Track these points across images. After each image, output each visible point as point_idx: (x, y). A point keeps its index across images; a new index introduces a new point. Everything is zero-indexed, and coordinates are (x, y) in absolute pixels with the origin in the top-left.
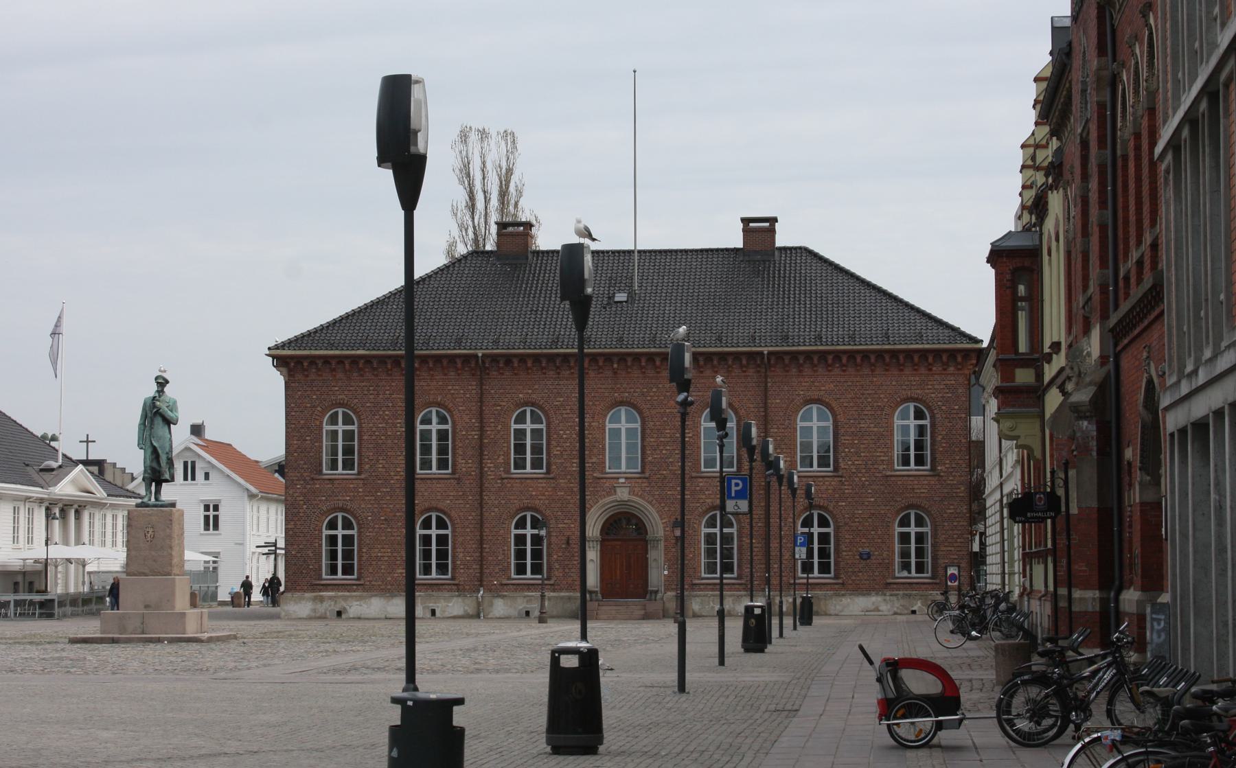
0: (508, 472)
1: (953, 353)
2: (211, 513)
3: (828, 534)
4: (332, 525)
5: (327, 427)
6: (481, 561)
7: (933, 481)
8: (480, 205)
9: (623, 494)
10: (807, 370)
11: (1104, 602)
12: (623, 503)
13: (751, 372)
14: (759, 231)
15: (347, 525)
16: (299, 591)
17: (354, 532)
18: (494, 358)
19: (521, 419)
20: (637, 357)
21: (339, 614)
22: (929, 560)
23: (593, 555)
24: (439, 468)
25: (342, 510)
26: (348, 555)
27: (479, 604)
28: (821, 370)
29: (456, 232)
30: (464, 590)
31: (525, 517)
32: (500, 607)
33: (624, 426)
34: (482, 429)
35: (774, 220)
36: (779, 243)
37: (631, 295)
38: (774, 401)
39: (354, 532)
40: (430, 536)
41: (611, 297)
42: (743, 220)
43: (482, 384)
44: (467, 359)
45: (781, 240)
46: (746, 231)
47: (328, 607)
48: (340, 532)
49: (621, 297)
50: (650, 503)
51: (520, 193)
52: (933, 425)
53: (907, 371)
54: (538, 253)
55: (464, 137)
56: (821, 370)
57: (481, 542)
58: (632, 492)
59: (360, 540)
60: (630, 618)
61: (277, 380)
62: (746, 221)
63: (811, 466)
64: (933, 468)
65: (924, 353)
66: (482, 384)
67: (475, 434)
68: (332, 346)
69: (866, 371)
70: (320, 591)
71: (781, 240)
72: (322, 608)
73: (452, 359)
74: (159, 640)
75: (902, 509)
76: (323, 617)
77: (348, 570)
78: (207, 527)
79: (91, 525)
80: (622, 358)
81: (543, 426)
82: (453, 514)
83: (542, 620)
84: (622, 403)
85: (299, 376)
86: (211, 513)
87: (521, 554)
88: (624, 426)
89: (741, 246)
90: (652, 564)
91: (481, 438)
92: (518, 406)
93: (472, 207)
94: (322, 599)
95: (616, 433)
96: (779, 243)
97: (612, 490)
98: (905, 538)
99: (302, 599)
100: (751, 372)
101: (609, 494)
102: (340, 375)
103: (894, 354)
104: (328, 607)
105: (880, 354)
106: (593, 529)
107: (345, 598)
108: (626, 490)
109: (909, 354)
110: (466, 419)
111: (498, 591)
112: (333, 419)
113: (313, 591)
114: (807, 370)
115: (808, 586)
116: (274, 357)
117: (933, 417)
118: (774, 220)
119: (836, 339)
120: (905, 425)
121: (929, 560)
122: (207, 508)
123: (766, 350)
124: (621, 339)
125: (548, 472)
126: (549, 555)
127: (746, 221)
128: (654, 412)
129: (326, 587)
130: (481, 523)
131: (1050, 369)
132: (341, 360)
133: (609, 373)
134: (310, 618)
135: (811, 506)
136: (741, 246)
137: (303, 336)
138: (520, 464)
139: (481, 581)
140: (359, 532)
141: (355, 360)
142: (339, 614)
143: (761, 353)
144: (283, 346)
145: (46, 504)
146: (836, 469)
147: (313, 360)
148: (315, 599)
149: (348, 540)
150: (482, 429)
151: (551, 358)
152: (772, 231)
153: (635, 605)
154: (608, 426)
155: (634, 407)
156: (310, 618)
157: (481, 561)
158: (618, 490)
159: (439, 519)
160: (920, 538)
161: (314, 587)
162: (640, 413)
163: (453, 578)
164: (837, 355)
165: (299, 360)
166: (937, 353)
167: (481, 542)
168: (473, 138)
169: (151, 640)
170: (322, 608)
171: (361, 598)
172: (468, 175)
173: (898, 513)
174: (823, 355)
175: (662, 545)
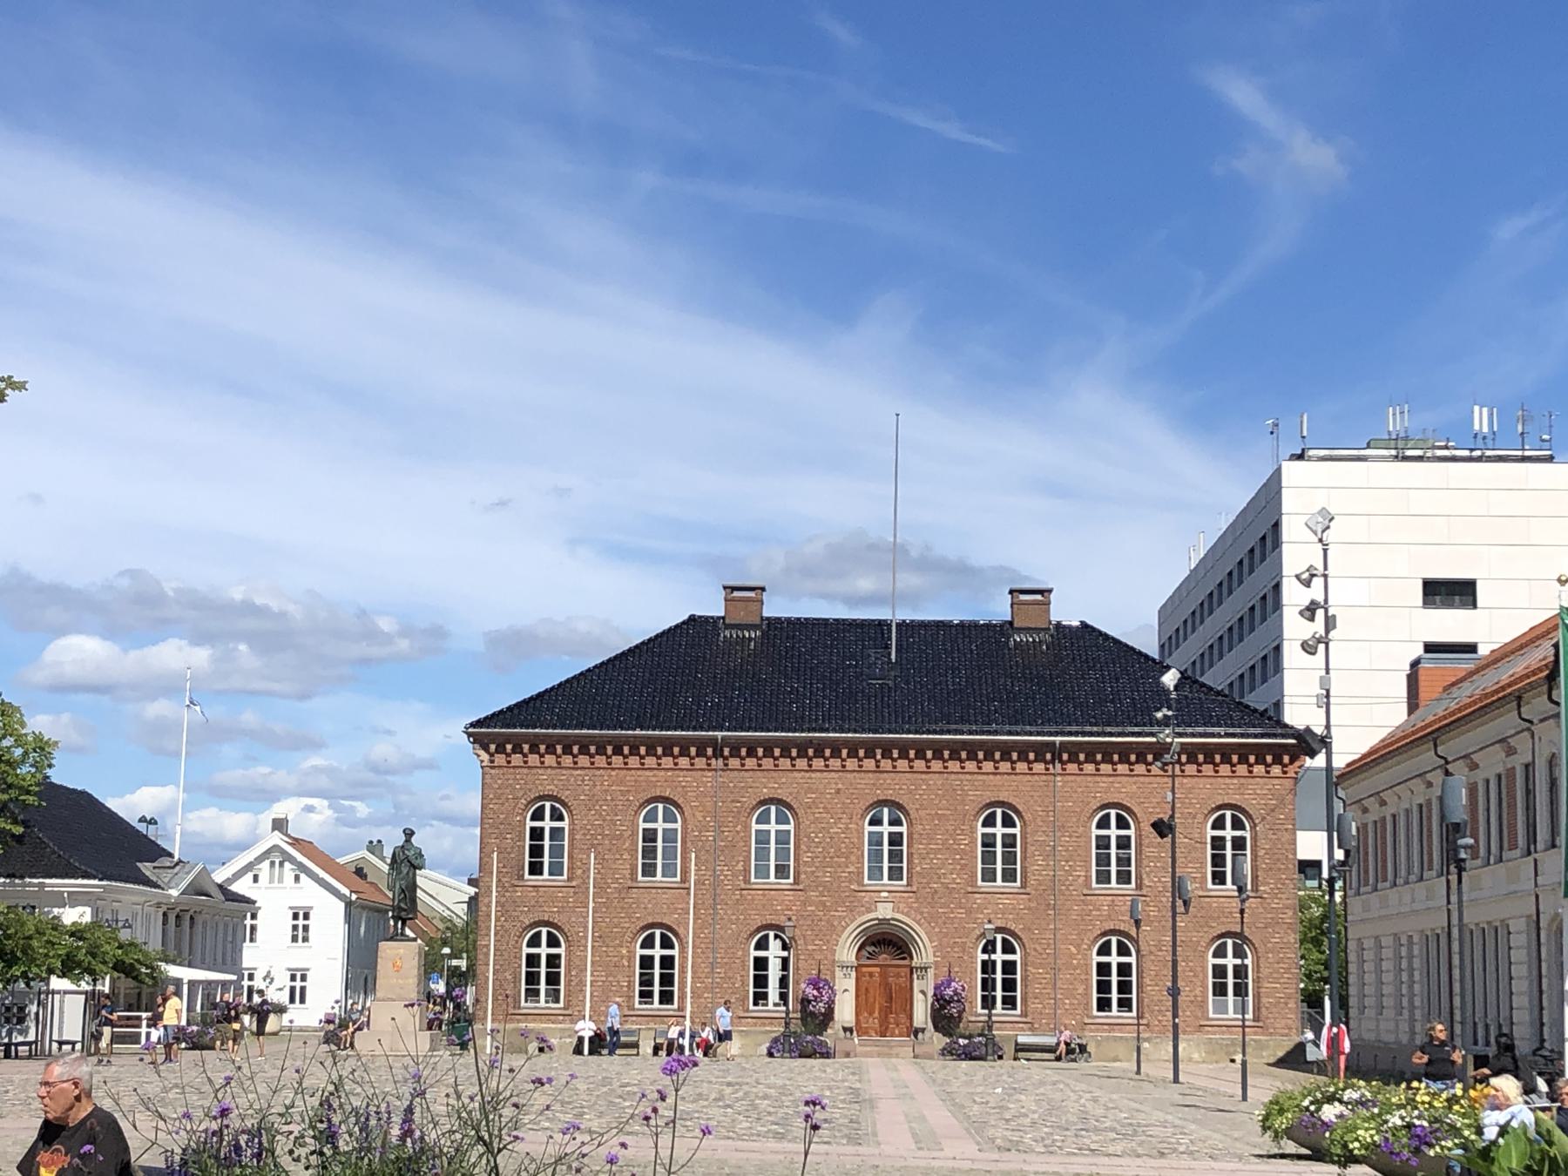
0: (747, 881)
2: (301, 922)
3: (558, 956)
9: (885, 911)
12: (883, 921)
19: (764, 819)
31: (539, 933)
40: (1225, 966)
42: (1011, 592)
59: (569, 961)
62: (1475, 606)
75: (758, 930)
78: (294, 939)
79: (204, 938)
81: (791, 827)
86: (301, 922)
98: (533, 960)
101: (869, 911)
110: (699, 816)
116: (469, 735)
122: (296, 916)
125: (796, 882)
127: (1475, 606)
145: (164, 908)
159: (1120, 944)
173: (752, 935)
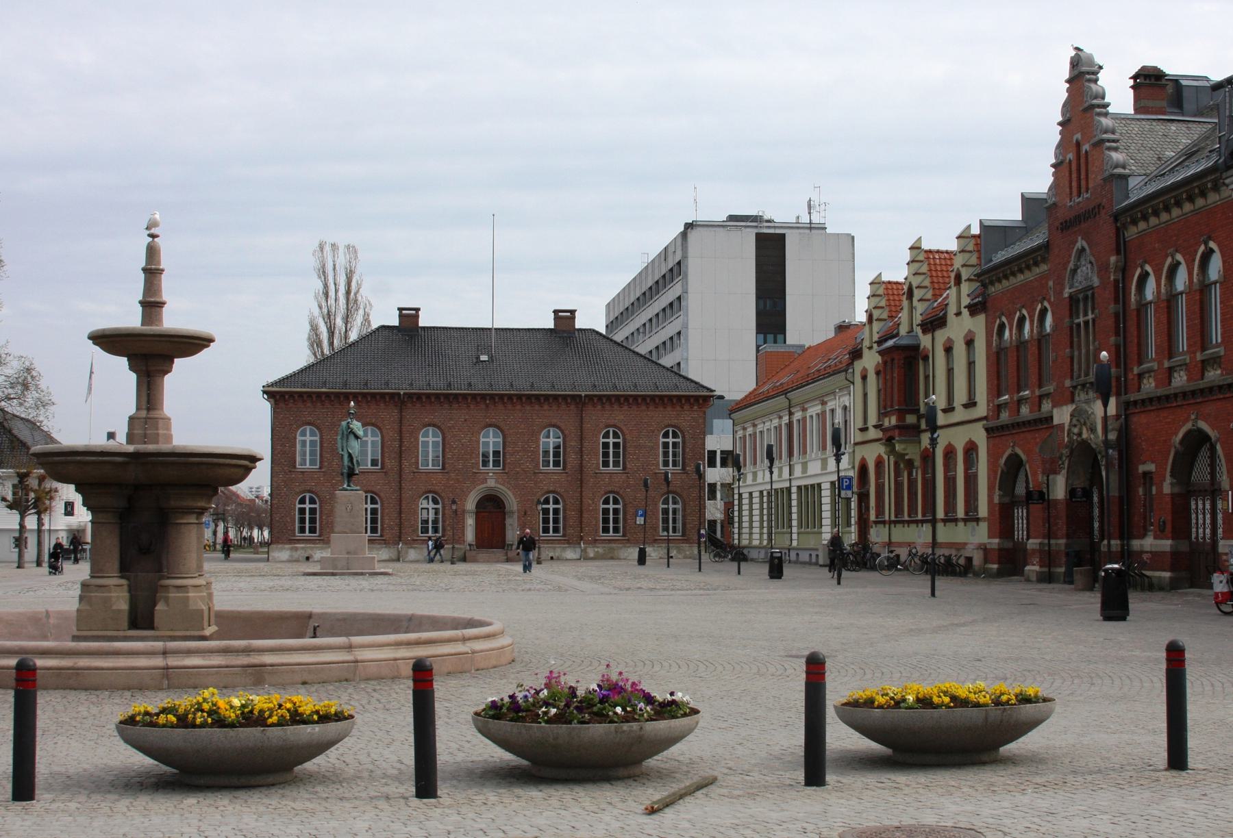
1: (697, 398)
4: (302, 501)
5: (299, 438)
6: (400, 525)
7: (684, 476)
8: (332, 293)
9: (491, 483)
10: (607, 407)
11: (1122, 546)
12: (491, 489)
13: (572, 407)
14: (409, 317)
15: (312, 501)
17: (316, 506)
18: (410, 396)
20: (501, 396)
21: (308, 558)
22: (440, 525)
23: (470, 522)
25: (309, 491)
26: (313, 521)
27: (399, 552)
28: (616, 407)
29: (316, 311)
32: (412, 554)
33: (431, 439)
34: (401, 441)
35: (417, 310)
36: (421, 324)
37: (491, 357)
38: (587, 426)
39: (316, 506)
41: (478, 358)
44: (392, 395)
45: (579, 324)
46: (401, 316)
47: (301, 554)
48: (307, 506)
49: (484, 358)
51: (359, 286)
52: (684, 442)
53: (669, 408)
54: (424, 328)
55: (321, 248)
56: (616, 407)
57: (400, 513)
58: (497, 482)
60: (498, 562)
61: (266, 407)
64: (684, 468)
65: (679, 398)
67: (397, 444)
68: (304, 386)
69: (644, 407)
71: (579, 324)
72: (296, 555)
73: (383, 395)
74: (362, 574)
76: (297, 561)
77: (313, 530)
80: (492, 396)
81: (620, 440)
83: (453, 563)
84: (490, 426)
85: (282, 405)
87: (606, 521)
88: (431, 439)
89: (397, 324)
90: (508, 527)
91: (400, 446)
93: (326, 295)
94: (296, 549)
95: (426, 444)
96: (421, 324)
97: (485, 481)
99: (282, 549)
100: (572, 407)
103: (661, 397)
104: (301, 554)
105: (653, 398)
106: (471, 504)
107: (312, 549)
109: (670, 398)
111: (412, 543)
114: (607, 407)
117: (683, 437)
118: (417, 310)
119: (625, 386)
120: (550, 440)
121: (440, 525)
123: (583, 394)
124: (532, 385)
126: (444, 521)
127: (556, 312)
129: (299, 541)
130: (400, 501)
132: (310, 395)
133: (483, 406)
134: (289, 561)
135: (668, 492)
136: (397, 324)
137: (284, 379)
138: (606, 464)
139: (400, 537)
140: (321, 507)
141: (319, 395)
142: (308, 558)
143: (580, 396)
144: (272, 385)
146: (624, 468)
147: (291, 394)
148: (291, 549)
149: (313, 511)
150: (401, 441)
151: (447, 396)
152: (417, 316)
153: (499, 553)
154: (482, 440)
155: (498, 428)
156: (289, 561)
157: (400, 525)
161: (291, 541)
162: (502, 431)
163: (564, 535)
164: (627, 398)
165: (282, 394)
166: (688, 398)
167: (400, 513)
168: (327, 248)
169: (356, 574)
170: (296, 555)
171: (322, 549)
172: (324, 272)
174: (618, 397)
175: (516, 516)
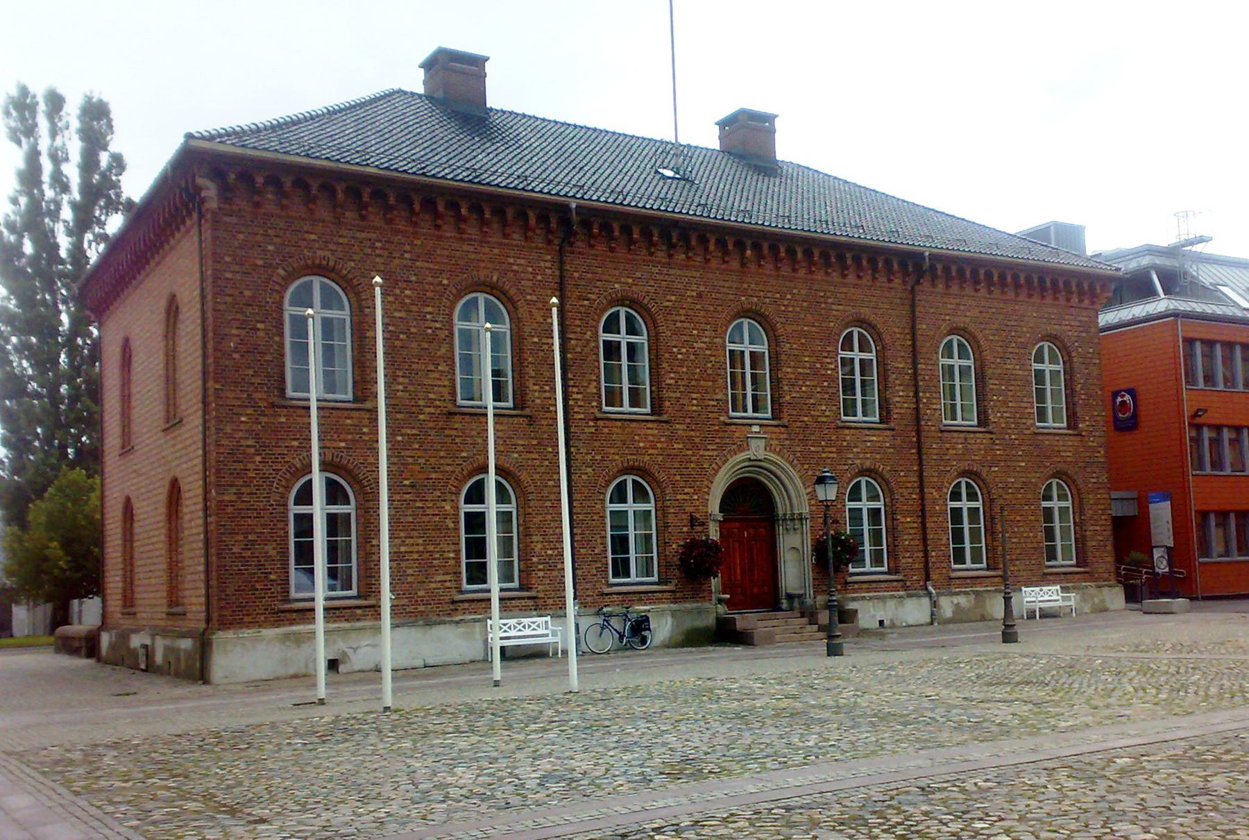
12: (754, 463)
16: (249, 625)
24: (631, 406)
30: (545, 606)
43: (562, 263)
50: (791, 463)
58: (769, 447)
63: (745, 411)
66: (562, 263)
70: (292, 622)
82: (524, 476)
92: (613, 302)
101: (741, 449)
102: (324, 213)
108: (762, 443)
112: (612, 325)
113: (277, 623)
115: (629, 598)
128: (790, 329)
131: (207, 188)
158: (753, 443)
160: (874, 513)
